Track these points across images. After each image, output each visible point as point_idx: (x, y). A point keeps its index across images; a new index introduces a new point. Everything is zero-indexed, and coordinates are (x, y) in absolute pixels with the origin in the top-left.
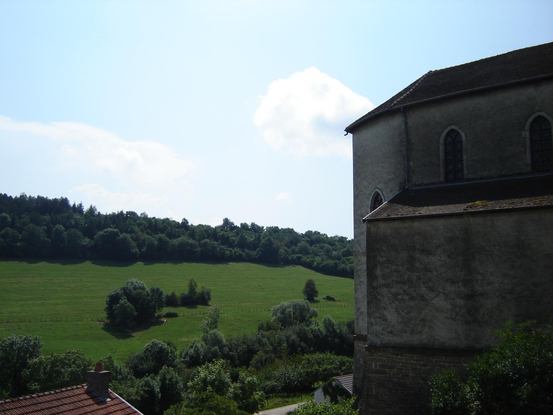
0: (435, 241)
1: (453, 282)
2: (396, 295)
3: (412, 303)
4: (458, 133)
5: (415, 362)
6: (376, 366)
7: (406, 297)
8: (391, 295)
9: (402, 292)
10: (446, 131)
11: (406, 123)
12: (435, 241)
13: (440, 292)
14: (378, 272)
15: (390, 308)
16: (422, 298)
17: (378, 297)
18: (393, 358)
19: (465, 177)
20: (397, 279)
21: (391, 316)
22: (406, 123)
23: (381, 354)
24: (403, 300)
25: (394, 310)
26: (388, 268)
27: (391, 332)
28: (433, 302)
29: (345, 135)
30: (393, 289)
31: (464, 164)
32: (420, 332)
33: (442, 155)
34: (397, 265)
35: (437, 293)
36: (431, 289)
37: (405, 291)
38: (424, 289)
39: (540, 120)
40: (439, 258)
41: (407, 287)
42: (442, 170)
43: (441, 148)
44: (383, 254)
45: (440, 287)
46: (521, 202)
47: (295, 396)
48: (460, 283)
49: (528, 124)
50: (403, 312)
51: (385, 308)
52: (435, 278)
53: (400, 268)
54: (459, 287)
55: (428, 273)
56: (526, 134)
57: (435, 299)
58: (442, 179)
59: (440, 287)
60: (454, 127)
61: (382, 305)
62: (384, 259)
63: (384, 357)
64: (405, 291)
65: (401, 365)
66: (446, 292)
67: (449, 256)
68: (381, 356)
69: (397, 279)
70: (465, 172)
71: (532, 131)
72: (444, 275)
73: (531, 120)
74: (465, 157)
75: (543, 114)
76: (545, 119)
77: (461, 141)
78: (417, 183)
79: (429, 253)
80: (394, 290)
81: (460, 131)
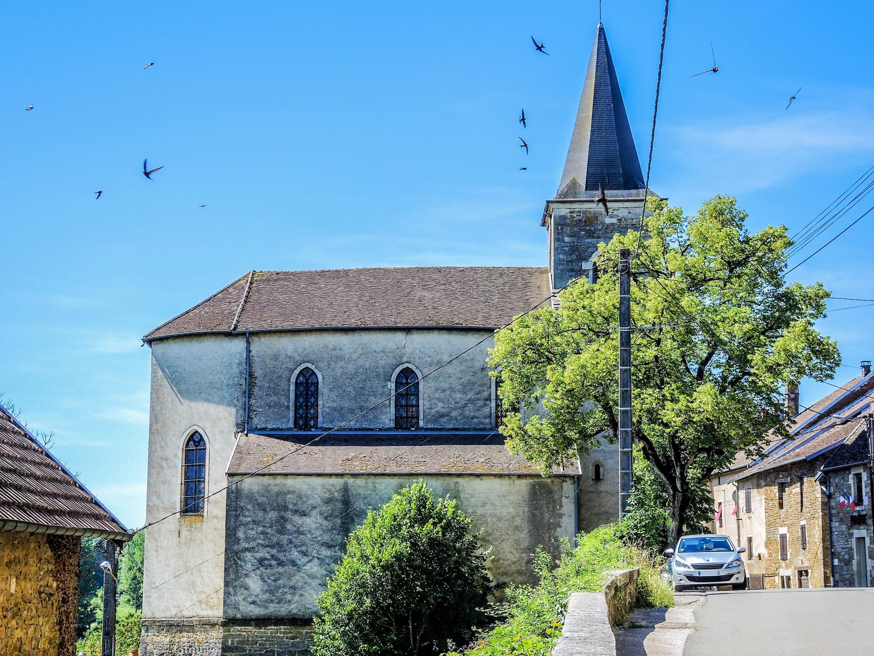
0: (311, 501)
1: (330, 547)
2: (261, 561)
3: (281, 569)
4: (314, 373)
5: (282, 635)
6: (233, 643)
7: (273, 563)
8: (256, 561)
9: (269, 557)
10: (299, 369)
11: (249, 351)
12: (311, 501)
13: (314, 557)
14: (241, 534)
15: (254, 575)
16: (293, 563)
17: (239, 562)
18: (255, 632)
19: (319, 425)
20: (264, 542)
21: (254, 584)
22: (249, 351)
23: (239, 628)
24: (270, 566)
25: (258, 577)
26: (253, 529)
27: (254, 603)
28: (306, 567)
29: (142, 346)
30: (257, 554)
31: (319, 410)
32: (290, 601)
33: (292, 396)
34: (264, 526)
35: (311, 558)
36: (305, 554)
37: (272, 556)
38: (296, 553)
39: (407, 373)
40: (314, 520)
41: (275, 551)
42: (292, 414)
43: (292, 387)
44: (247, 513)
45: (315, 551)
46: (570, 527)
47: (267, 616)
48: (337, 548)
49: (395, 376)
50: (269, 579)
51: (247, 575)
52: (308, 542)
53: (269, 530)
54: (335, 552)
55: (301, 536)
56: (392, 385)
57: (308, 564)
58: (291, 425)
59: (315, 551)
60: (309, 365)
61: (244, 572)
62: (249, 519)
63: (244, 631)
64: (272, 556)
65: (264, 639)
66: (320, 557)
67: (326, 519)
68: (239, 631)
69: (264, 542)
70: (320, 419)
71: (398, 384)
72: (319, 539)
73: (398, 370)
74: (320, 403)
75: (410, 366)
76: (413, 372)
77: (317, 383)
78: (259, 427)
79: (304, 514)
80: (258, 555)
81: (317, 371)
